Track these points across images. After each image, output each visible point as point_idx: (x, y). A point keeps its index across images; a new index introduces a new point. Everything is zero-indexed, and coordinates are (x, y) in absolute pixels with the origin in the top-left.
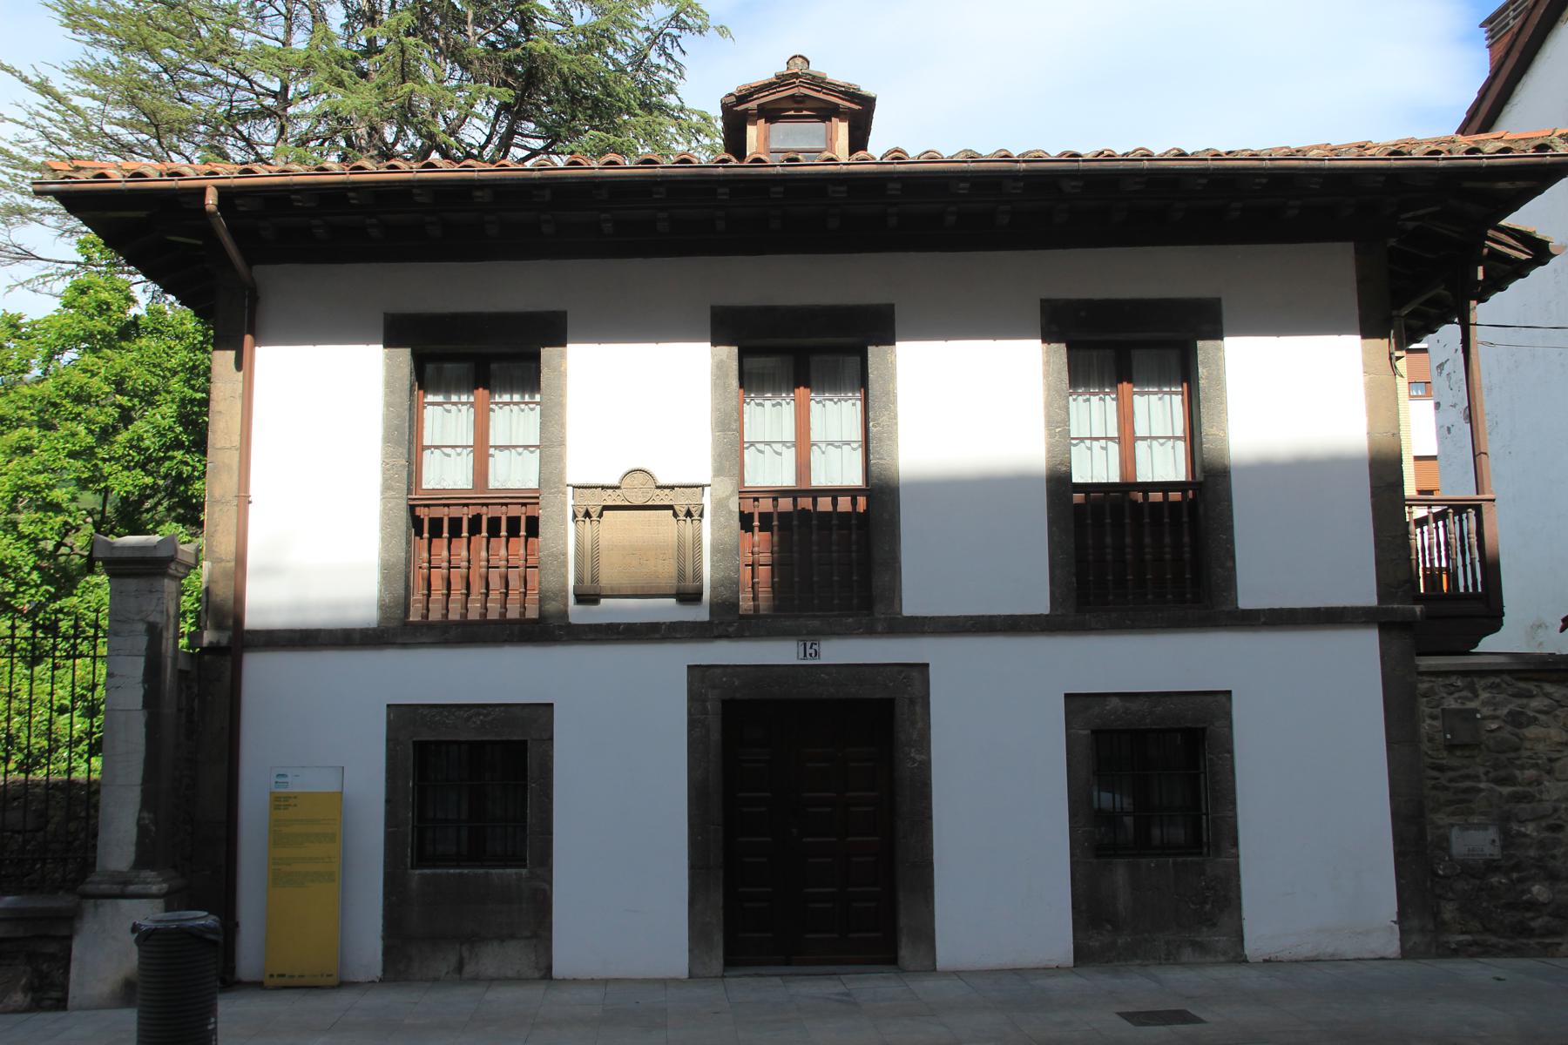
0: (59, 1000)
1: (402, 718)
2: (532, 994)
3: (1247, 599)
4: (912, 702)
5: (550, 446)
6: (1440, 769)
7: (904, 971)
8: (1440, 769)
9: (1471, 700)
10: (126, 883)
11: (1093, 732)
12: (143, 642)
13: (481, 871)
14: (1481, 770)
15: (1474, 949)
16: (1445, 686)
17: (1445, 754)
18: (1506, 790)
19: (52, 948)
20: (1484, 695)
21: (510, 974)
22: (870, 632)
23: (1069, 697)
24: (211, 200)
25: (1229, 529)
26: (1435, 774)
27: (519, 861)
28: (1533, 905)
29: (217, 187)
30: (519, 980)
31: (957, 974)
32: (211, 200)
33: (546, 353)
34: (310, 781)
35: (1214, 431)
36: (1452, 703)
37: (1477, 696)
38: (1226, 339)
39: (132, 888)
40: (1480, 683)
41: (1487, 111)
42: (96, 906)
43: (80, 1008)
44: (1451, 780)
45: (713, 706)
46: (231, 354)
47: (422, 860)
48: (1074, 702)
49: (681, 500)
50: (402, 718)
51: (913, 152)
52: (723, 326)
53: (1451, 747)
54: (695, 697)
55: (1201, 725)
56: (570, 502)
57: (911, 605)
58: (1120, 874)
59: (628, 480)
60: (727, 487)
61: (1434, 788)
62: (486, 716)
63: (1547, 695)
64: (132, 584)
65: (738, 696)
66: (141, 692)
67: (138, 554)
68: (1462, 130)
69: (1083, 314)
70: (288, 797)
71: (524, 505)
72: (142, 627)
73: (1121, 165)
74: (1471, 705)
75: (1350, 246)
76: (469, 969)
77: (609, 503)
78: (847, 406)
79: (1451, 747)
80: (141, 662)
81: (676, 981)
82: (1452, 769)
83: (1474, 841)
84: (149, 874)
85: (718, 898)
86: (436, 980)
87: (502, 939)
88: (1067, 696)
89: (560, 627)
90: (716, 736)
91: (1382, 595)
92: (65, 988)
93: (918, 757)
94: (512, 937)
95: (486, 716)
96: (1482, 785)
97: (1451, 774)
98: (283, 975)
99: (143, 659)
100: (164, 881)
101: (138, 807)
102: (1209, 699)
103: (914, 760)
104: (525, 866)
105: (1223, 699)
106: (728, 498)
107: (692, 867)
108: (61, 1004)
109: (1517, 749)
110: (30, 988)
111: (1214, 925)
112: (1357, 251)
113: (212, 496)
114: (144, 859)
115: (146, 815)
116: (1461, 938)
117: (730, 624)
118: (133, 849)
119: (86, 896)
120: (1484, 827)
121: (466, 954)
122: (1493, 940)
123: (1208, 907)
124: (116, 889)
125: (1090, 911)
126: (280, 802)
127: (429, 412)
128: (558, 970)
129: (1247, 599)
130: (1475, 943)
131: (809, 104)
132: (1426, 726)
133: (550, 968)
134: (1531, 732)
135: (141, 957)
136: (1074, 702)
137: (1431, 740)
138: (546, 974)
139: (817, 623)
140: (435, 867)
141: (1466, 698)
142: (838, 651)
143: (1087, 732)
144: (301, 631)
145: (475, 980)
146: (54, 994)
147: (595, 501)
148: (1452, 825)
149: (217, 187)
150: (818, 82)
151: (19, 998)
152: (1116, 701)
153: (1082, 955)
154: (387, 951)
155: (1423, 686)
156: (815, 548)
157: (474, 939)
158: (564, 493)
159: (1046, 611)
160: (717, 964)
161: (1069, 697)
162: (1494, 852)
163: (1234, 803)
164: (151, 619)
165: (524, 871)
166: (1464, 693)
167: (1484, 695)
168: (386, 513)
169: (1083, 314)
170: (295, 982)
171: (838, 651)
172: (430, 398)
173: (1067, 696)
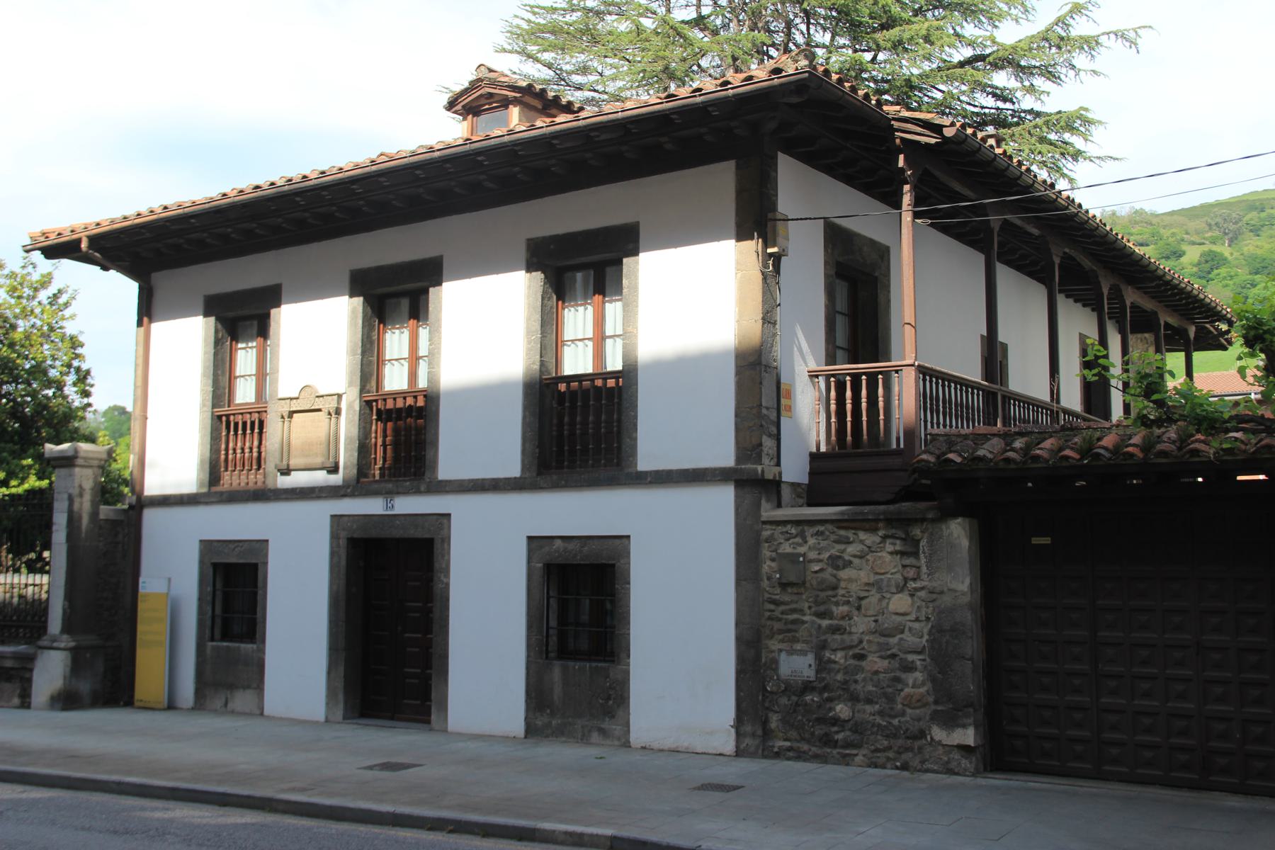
1: (208, 547)
4: (443, 540)
9: (800, 545)
15: (791, 754)
18: (825, 623)
20: (812, 541)
26: (772, 607)
28: (836, 721)
30: (249, 714)
36: (786, 548)
40: (810, 531)
45: (343, 542)
50: (208, 547)
53: (784, 586)
54: (334, 536)
58: (556, 672)
61: (770, 618)
63: (862, 542)
72: (66, 496)
74: (802, 550)
79: (784, 586)
83: (796, 665)
88: (530, 538)
90: (343, 563)
94: (249, 687)
97: (783, 608)
120: (803, 653)
122: (805, 747)
128: (266, 712)
130: (790, 749)
133: (262, 709)
137: (769, 578)
138: (262, 714)
139: (390, 486)
151: (16, 701)
152: (558, 543)
157: (232, 687)
160: (339, 713)
166: (798, 540)
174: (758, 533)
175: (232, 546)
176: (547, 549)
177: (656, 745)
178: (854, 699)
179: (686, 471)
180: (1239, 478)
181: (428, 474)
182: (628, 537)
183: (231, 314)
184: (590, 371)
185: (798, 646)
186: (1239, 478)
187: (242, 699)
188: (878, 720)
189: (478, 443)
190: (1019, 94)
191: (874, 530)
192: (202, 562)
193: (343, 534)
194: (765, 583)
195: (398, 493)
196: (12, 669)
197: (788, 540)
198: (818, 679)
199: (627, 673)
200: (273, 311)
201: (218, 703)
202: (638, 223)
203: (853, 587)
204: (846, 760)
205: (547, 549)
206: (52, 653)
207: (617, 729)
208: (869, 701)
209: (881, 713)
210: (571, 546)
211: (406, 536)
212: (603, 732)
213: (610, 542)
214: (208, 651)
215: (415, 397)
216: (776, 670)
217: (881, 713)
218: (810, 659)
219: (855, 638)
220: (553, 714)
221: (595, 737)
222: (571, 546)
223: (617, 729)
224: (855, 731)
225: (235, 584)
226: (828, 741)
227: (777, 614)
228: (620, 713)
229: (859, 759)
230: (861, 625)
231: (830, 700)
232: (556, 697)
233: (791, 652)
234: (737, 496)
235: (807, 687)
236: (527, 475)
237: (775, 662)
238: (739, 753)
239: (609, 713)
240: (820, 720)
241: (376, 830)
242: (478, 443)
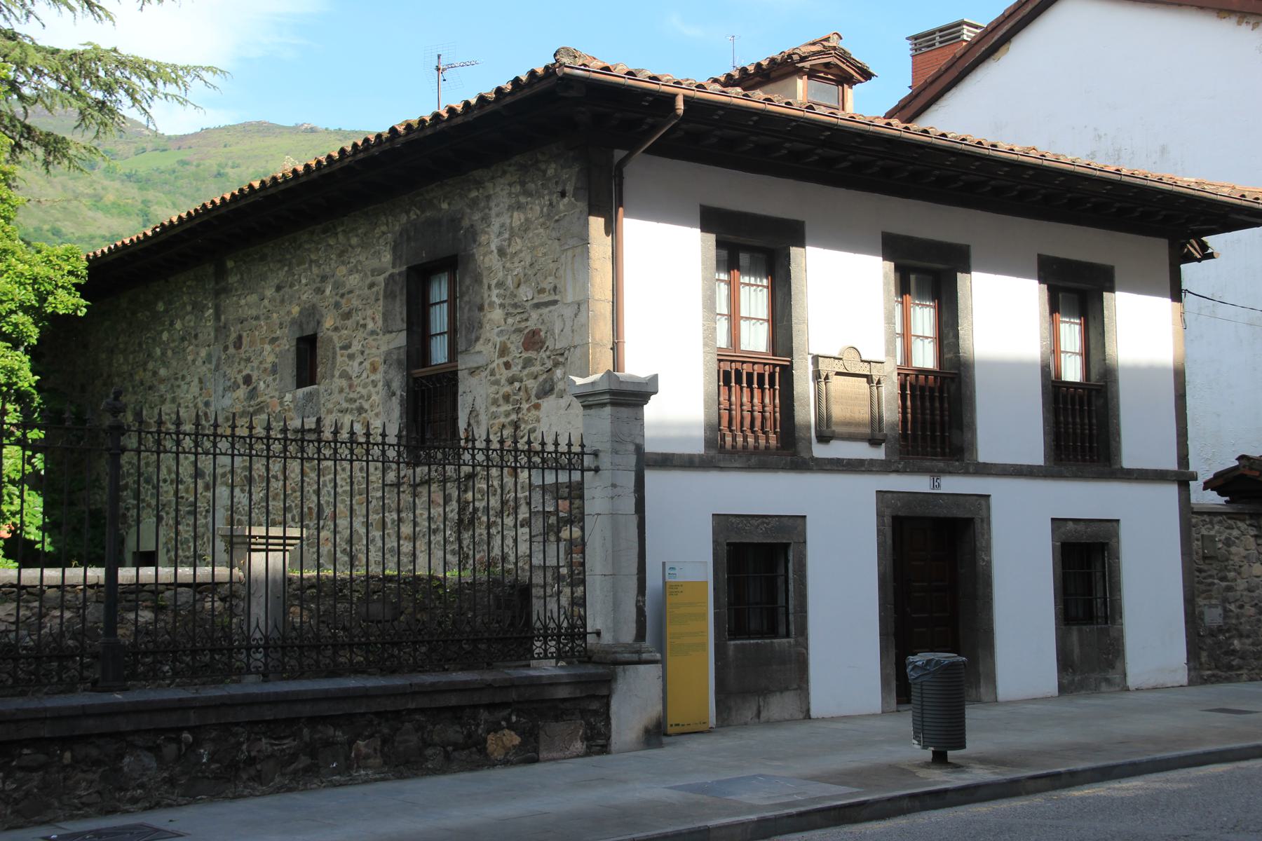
0: (602, 746)
1: (722, 523)
2: (803, 729)
3: (1128, 462)
4: (982, 520)
14: (1215, 572)
18: (1224, 584)
19: (595, 706)
21: (787, 717)
25: (1117, 416)
28: (1234, 652)
29: (685, 96)
30: (792, 720)
31: (1008, 703)
32: (680, 105)
33: (794, 251)
38: (973, 273)
40: (1216, 519)
41: (914, 106)
42: (624, 671)
43: (619, 752)
45: (888, 520)
46: (601, 221)
50: (722, 523)
51: (1003, 146)
52: (710, 220)
53: (1205, 558)
57: (985, 454)
63: (1238, 528)
64: (592, 412)
66: (634, 501)
67: (636, 389)
68: (890, 115)
71: (732, 361)
72: (632, 448)
73: (1138, 181)
74: (1212, 533)
76: (764, 715)
78: (927, 310)
81: (874, 715)
83: (1213, 616)
86: (746, 724)
88: (1053, 520)
90: (889, 542)
92: (608, 738)
94: (787, 689)
97: (1204, 574)
105: (799, 521)
107: (881, 635)
108: (605, 749)
109: (1227, 560)
110: (587, 738)
113: (594, 339)
116: (1209, 672)
118: (634, 625)
122: (1220, 673)
124: (635, 657)
125: (1065, 662)
127: (744, 291)
128: (813, 714)
129: (1128, 462)
130: (1213, 675)
131: (834, 71)
133: (808, 710)
134: (1233, 549)
138: (807, 716)
139: (941, 464)
140: (750, 638)
145: (770, 723)
146: (601, 742)
149: (685, 96)
150: (845, 56)
151: (579, 746)
152: (1071, 523)
153: (1062, 689)
157: (764, 692)
160: (893, 701)
162: (1220, 621)
165: (792, 640)
167: (1217, 527)
168: (706, 363)
170: (686, 729)
172: (746, 279)
173: (1053, 520)
175: (755, 522)
176: (1063, 530)
177: (1144, 686)
178: (1241, 636)
179: (832, 459)
181: (967, 455)
183: (731, 238)
184: (1078, 380)
185: (1214, 602)
187: (779, 705)
188: (1251, 648)
189: (1009, 426)
191: (1243, 520)
193: (888, 512)
194: (1195, 557)
195: (950, 473)
196: (564, 700)
198: (1226, 624)
199: (1121, 631)
200: (961, 277)
201: (749, 714)
203: (1236, 559)
204: (1238, 679)
206: (642, 667)
207: (1116, 677)
208: (1248, 636)
209: (1253, 644)
210: (1081, 527)
211: (949, 515)
212: (1108, 681)
213: (1103, 524)
214: (731, 653)
215: (926, 377)
216: (1202, 620)
217: (1253, 644)
218: (1220, 610)
219: (1239, 593)
220: (1074, 672)
221: (1104, 687)
223: (1116, 677)
224: (1242, 658)
225: (759, 569)
226: (1230, 667)
228: (1118, 664)
229: (1244, 677)
230: (1241, 585)
231: (1230, 638)
235: (1220, 630)
237: (1202, 613)
238: (1191, 683)
239: (1111, 665)
240: (1226, 653)
241: (901, 822)
242: (1009, 426)
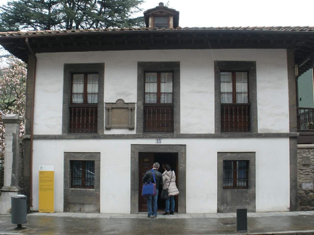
1: (67, 154)
5: (101, 94)
6: (301, 170)
7: (178, 213)
8: (301, 170)
9: (309, 154)
10: (10, 189)
11: (224, 161)
12: (12, 137)
13: (85, 189)
15: (306, 209)
16: (303, 151)
17: (302, 166)
20: (312, 153)
22: (173, 137)
23: (218, 153)
24: (27, 40)
26: (300, 171)
27: (92, 187)
32: (27, 40)
34: (48, 168)
35: (253, 92)
36: (304, 155)
37: (310, 153)
39: (11, 190)
40: (311, 150)
44: (303, 172)
47: (72, 186)
48: (220, 154)
49: (130, 106)
50: (67, 154)
53: (304, 165)
54: (132, 152)
55: (249, 160)
56: (105, 106)
57: (184, 130)
58: (228, 193)
59: (118, 102)
60: (141, 103)
61: (300, 174)
62: (85, 155)
65: (142, 151)
69: (224, 64)
70: (43, 172)
72: (12, 134)
74: (309, 156)
75: (286, 50)
77: (113, 107)
79: (304, 165)
80: (12, 142)
82: (304, 170)
84: (14, 187)
85: (137, 196)
87: (89, 204)
89: (102, 135)
90: (137, 160)
91: (291, 130)
93: (183, 166)
94: (91, 204)
95: (85, 155)
96: (310, 173)
97: (304, 171)
98: (42, 210)
99: (12, 141)
100: (17, 189)
101: (11, 173)
102: (95, 154)
103: (182, 167)
104: (94, 189)
106: (141, 106)
111: (249, 204)
112: (287, 51)
114: (13, 184)
115: (13, 174)
117: (140, 135)
119: (2, 191)
120: (309, 182)
121: (81, 207)
123: (248, 200)
126: (41, 173)
132: (299, 160)
135: (12, 206)
136: (220, 154)
137: (300, 163)
139: (160, 135)
141: (307, 154)
142: (165, 142)
143: (222, 161)
144: (222, 169)
147: (110, 106)
148: (303, 182)
152: (229, 154)
154: (64, 206)
155: (298, 151)
156: (161, 118)
158: (104, 105)
159: (214, 133)
161: (218, 153)
163: (255, 177)
164: (14, 132)
165: (94, 189)
166: (308, 153)
169: (224, 64)
171: (165, 142)
174: (296, 151)
176: (225, 156)
180: (25, 49)
182: (255, 152)
186: (25, 49)
190: (4, 61)
192: (65, 160)
197: (304, 153)
202: (180, 62)
205: (225, 156)
222: (233, 155)
227: (302, 172)
232: (228, 200)
233: (306, 183)
234: (290, 141)
236: (217, 133)
